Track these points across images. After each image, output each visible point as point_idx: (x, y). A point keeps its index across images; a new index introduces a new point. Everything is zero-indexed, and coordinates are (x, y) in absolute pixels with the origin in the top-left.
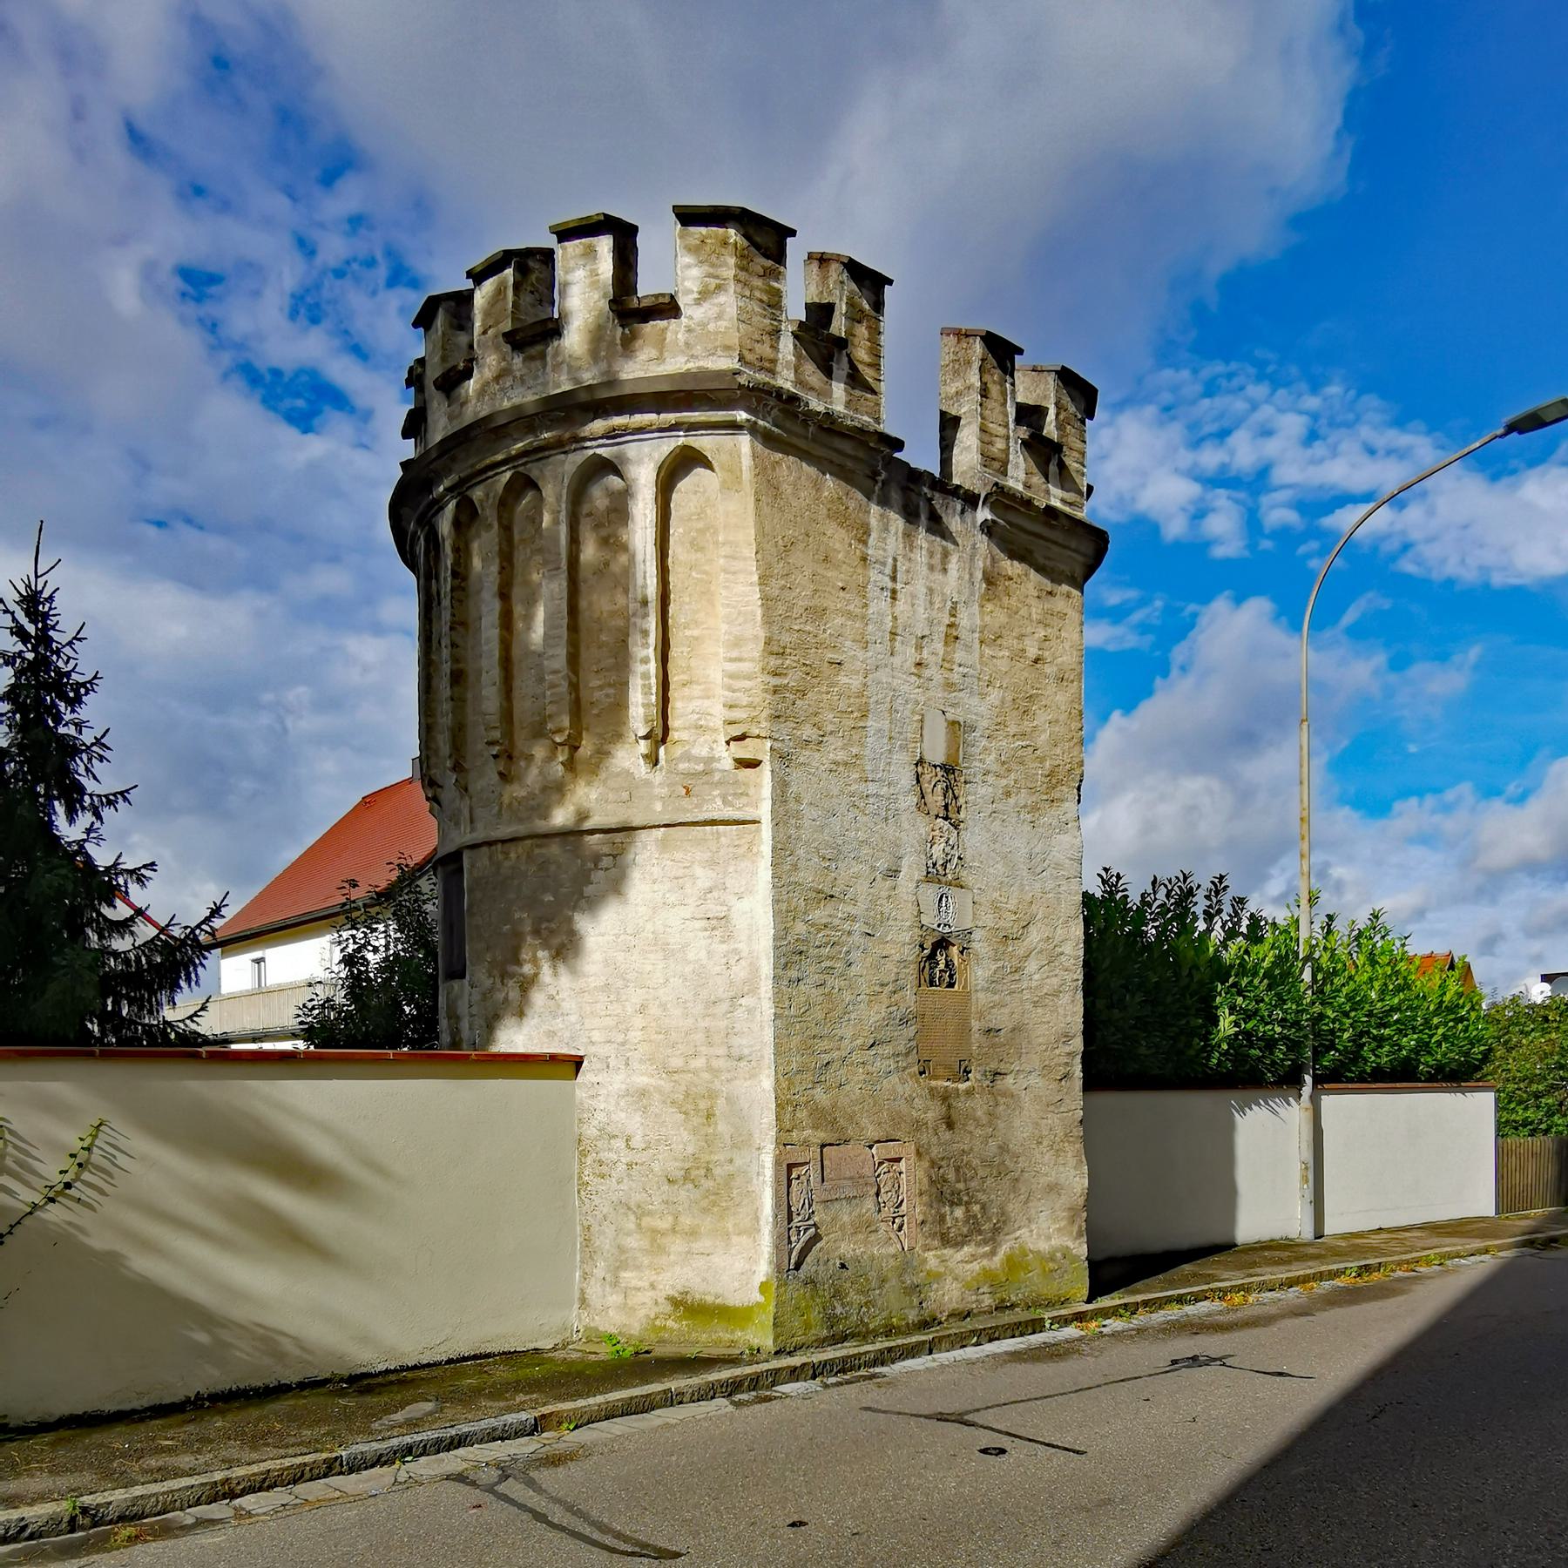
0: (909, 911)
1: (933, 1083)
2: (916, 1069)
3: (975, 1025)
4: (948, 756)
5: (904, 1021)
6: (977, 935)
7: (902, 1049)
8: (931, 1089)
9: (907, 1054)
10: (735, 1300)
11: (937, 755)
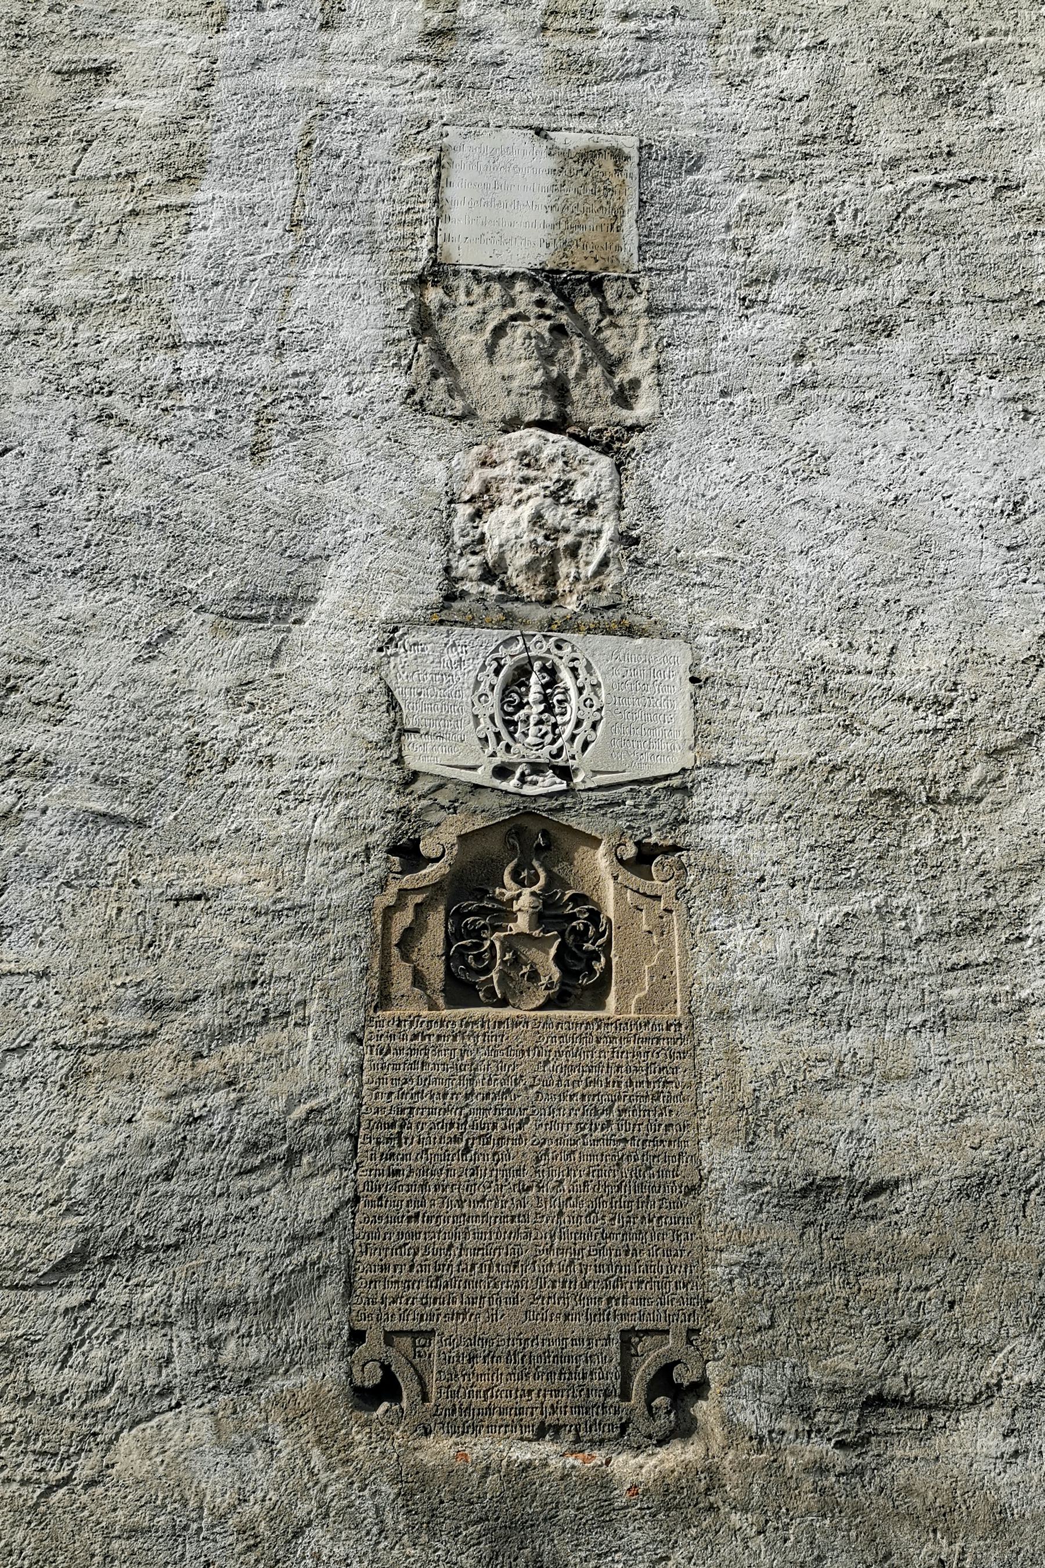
0: (341, 738)
1: (438, 1449)
2: (329, 1373)
3: (723, 1161)
4: (566, 219)
5: (273, 1151)
6: (722, 795)
7: (249, 1278)
8: (414, 1487)
9: (278, 1305)
10: (410, 971)
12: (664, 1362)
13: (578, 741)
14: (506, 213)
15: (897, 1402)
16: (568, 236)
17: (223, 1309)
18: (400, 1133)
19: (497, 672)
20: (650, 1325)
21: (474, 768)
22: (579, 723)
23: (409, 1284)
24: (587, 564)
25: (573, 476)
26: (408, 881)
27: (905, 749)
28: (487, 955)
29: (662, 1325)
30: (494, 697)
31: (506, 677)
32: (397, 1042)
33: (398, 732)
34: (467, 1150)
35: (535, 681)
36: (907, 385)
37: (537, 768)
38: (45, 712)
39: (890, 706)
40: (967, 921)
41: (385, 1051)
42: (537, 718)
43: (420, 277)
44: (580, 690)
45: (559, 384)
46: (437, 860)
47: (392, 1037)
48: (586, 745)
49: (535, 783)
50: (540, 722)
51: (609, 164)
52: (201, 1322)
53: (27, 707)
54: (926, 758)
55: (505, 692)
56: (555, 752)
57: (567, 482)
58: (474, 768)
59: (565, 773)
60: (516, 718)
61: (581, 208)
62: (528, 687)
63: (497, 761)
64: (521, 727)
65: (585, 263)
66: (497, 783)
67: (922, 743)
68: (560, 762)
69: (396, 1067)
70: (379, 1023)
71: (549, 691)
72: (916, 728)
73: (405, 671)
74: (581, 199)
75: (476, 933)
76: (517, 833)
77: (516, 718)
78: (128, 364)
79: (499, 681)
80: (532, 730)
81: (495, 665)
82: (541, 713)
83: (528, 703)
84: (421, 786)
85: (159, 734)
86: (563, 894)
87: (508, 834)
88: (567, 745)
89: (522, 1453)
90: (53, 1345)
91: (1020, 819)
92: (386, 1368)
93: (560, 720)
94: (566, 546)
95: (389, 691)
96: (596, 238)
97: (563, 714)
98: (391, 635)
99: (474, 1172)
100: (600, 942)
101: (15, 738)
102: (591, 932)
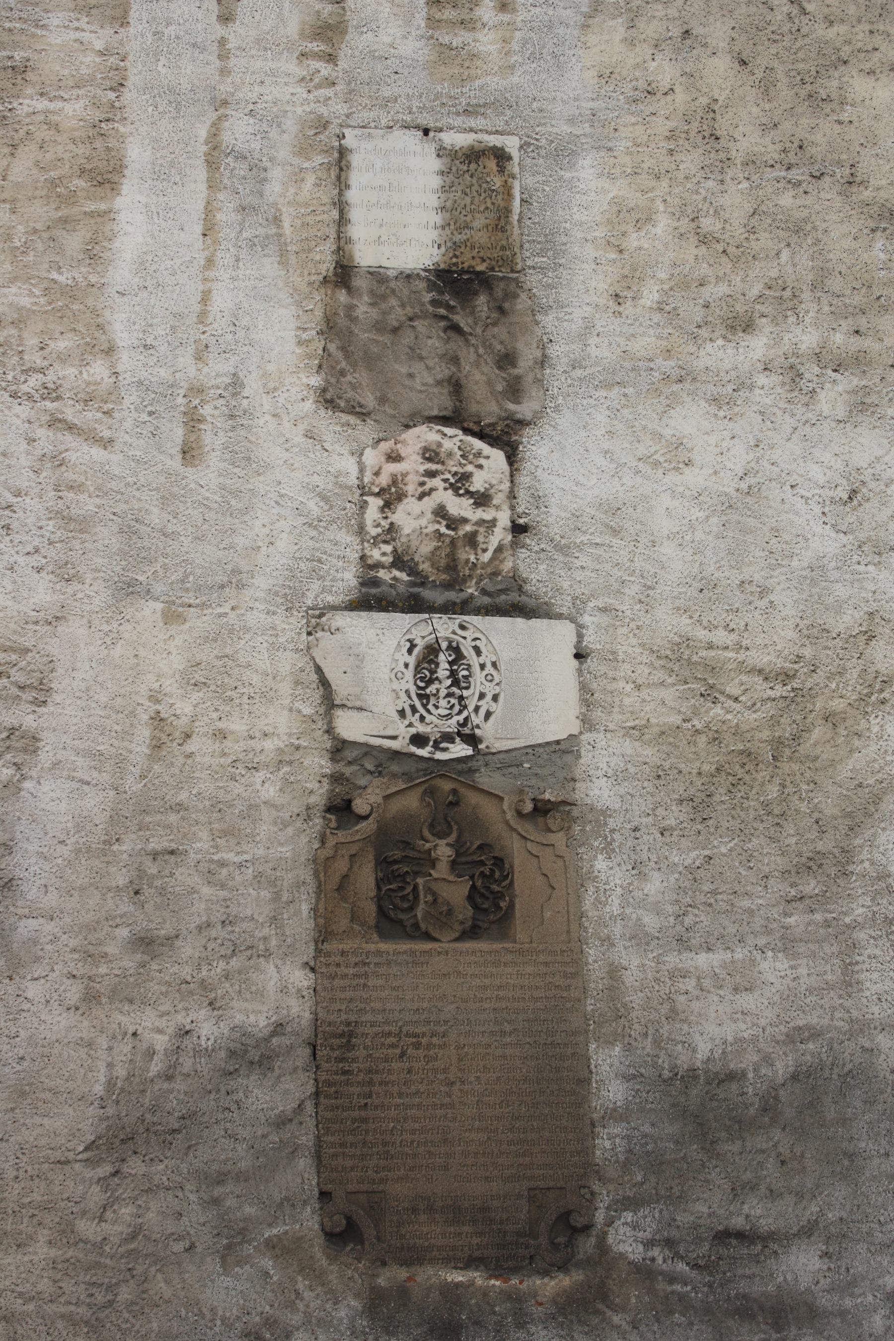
4: (454, 218)
12: (562, 1210)
13: (482, 712)
14: (402, 223)
15: (740, 1235)
16: (457, 238)
17: (221, 1179)
18: (349, 1041)
19: (410, 651)
20: (552, 1184)
21: (394, 738)
22: (482, 696)
23: (363, 1157)
24: (485, 550)
25: (470, 468)
26: (342, 836)
27: (755, 716)
28: (411, 897)
29: (561, 1184)
30: (409, 674)
31: (418, 656)
32: (343, 970)
33: (330, 702)
34: (402, 1055)
35: (443, 659)
36: (762, 380)
37: (448, 737)
38: (28, 696)
39: (744, 678)
40: (804, 860)
41: (332, 977)
42: (446, 691)
43: (325, 277)
44: (483, 667)
45: (453, 381)
46: (366, 817)
47: (338, 965)
48: (488, 715)
49: (445, 750)
50: (449, 695)
51: (492, 164)
52: (204, 1187)
53: (14, 690)
54: (774, 721)
55: (418, 669)
56: (462, 722)
57: (463, 474)
58: (394, 738)
59: (472, 740)
60: (428, 691)
61: (468, 209)
62: (437, 665)
63: (413, 731)
64: (433, 700)
65: (473, 263)
66: (413, 749)
67: (770, 709)
68: (466, 731)
69: (343, 989)
70: (328, 955)
71: (455, 667)
72: (765, 696)
73: (330, 653)
74: (468, 200)
75: (403, 877)
76: (431, 792)
77: (428, 691)
78: (71, 371)
79: (412, 660)
80: (443, 703)
81: (408, 645)
82: (449, 687)
83: (437, 679)
84: (350, 754)
85: (126, 712)
86: (472, 844)
87: (425, 793)
88: (473, 716)
89: (458, 1277)
90: (91, 1205)
91: (849, 774)
92: (349, 1219)
93: (465, 693)
94: (465, 535)
95: (319, 670)
96: (482, 238)
97: (467, 688)
98: (316, 619)
99: (409, 1071)
100: (504, 884)
101: (9, 719)
102: (497, 874)
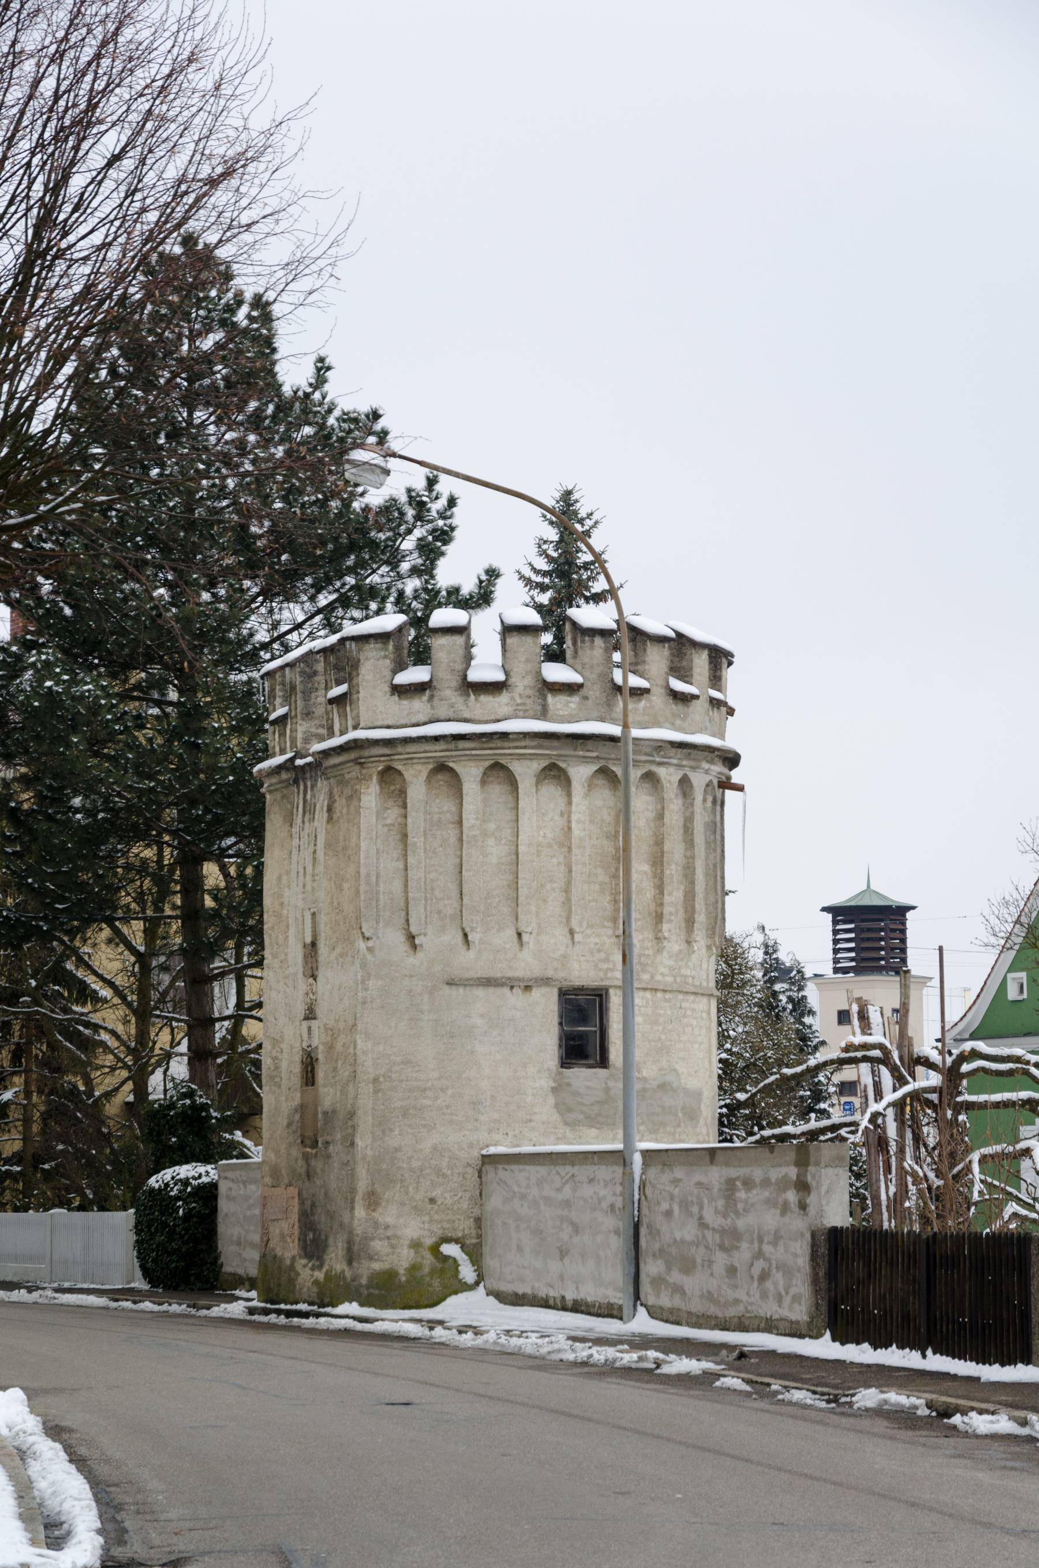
11: (308, 940)
